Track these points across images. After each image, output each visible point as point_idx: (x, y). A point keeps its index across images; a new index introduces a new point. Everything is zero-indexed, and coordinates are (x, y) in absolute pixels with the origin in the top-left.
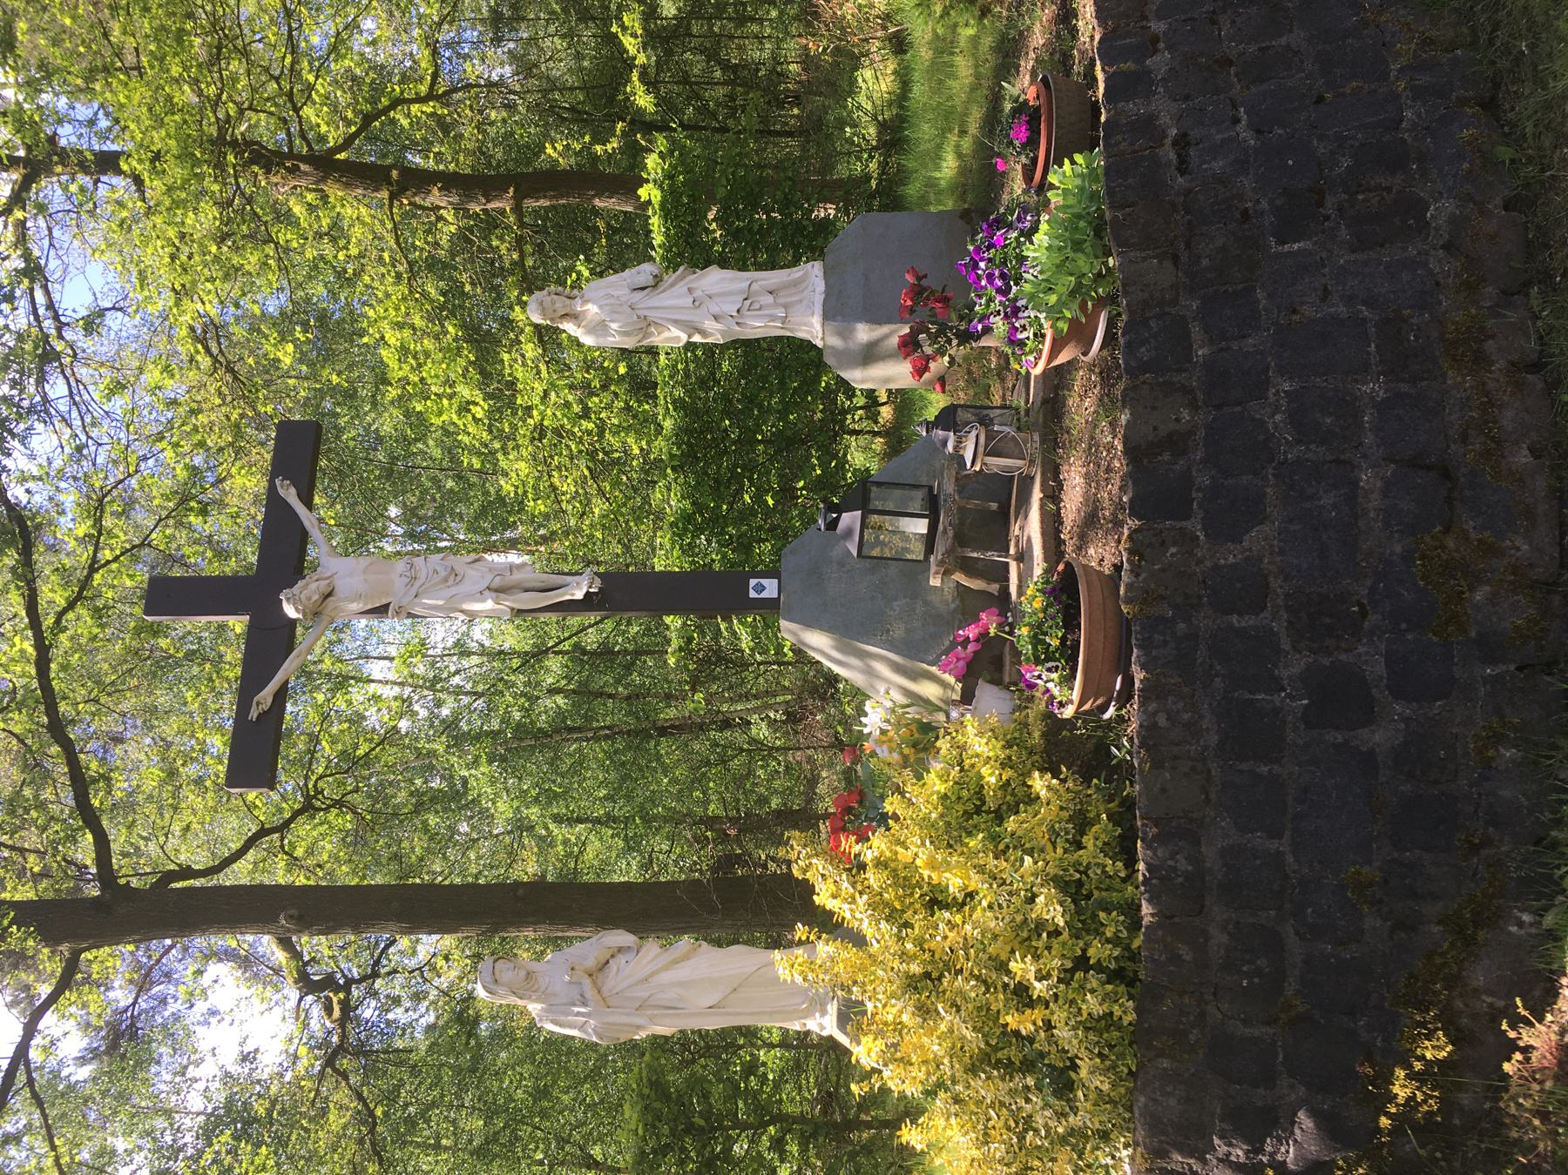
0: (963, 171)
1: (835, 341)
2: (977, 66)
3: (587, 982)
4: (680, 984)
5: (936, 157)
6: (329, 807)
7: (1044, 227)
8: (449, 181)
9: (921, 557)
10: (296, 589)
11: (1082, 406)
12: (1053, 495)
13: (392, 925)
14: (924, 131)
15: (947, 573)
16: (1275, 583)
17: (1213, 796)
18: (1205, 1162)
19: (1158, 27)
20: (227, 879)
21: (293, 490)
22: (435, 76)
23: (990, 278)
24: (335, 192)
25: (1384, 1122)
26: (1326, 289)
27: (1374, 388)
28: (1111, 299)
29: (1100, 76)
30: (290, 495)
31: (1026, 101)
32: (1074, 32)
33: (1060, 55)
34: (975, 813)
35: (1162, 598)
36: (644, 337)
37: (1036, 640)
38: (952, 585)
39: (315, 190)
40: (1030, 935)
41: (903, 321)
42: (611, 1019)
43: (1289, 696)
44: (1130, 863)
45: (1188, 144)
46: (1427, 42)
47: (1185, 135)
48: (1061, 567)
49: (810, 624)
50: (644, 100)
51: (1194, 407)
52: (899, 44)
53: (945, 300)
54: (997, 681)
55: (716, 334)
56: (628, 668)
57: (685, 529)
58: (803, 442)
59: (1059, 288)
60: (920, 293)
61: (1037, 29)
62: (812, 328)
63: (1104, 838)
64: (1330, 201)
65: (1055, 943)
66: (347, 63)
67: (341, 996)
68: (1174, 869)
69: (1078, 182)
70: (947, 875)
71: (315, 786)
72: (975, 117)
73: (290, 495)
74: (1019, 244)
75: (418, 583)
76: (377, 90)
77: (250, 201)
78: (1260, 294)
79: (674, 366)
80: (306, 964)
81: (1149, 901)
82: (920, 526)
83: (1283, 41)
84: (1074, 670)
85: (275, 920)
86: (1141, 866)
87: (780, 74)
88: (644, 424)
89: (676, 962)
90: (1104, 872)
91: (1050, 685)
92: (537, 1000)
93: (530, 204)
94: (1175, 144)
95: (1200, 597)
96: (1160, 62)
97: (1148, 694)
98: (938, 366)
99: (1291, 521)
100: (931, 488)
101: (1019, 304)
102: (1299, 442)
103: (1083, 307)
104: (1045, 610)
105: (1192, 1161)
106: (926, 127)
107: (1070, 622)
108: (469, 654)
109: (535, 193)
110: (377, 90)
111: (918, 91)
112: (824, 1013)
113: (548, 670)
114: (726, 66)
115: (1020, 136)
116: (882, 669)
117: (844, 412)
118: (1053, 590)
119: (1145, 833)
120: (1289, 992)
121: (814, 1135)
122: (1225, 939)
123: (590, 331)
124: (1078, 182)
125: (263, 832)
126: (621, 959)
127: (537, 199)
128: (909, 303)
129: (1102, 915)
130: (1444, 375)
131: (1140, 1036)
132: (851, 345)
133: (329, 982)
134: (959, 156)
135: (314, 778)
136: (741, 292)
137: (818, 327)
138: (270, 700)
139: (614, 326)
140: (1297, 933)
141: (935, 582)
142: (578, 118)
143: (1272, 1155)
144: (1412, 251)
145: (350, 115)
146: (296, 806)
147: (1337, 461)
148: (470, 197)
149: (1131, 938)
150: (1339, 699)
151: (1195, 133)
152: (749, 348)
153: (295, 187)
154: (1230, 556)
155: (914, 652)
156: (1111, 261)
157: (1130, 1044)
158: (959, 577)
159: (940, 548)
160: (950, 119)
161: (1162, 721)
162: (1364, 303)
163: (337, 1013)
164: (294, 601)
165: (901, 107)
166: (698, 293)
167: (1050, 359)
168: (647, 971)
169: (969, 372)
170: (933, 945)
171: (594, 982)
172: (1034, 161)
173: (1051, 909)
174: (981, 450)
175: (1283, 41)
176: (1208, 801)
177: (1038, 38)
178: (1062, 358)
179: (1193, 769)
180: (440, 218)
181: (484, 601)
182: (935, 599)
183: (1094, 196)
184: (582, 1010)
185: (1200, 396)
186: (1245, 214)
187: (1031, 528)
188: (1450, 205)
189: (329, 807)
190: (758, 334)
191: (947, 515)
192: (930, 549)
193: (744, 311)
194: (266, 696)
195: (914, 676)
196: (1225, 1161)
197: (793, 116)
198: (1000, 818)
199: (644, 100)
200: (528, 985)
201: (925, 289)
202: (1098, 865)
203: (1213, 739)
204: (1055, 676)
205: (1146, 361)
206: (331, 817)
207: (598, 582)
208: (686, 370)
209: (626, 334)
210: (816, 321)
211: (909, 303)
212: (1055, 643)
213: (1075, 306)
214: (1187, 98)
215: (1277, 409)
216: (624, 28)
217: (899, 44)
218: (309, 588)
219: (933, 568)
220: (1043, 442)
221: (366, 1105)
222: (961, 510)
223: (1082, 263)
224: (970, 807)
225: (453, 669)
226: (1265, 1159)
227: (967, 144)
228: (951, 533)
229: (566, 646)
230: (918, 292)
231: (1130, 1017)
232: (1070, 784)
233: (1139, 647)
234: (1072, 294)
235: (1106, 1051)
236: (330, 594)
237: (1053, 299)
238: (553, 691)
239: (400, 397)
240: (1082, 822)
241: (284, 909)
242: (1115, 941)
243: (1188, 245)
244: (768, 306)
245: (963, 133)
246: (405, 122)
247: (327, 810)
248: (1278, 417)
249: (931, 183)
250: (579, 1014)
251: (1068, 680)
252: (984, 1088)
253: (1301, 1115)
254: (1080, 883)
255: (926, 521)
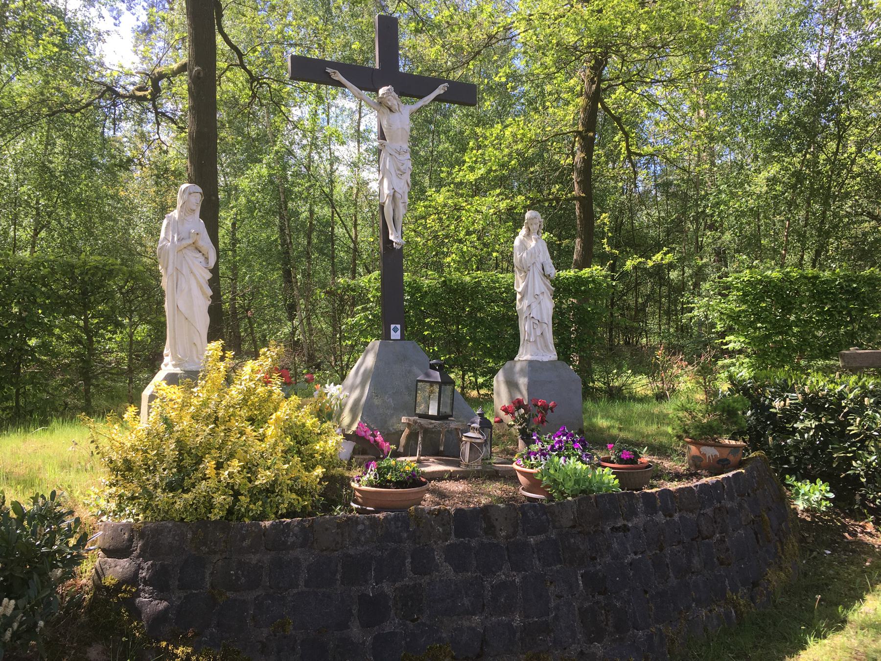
0: (601, 430)
1: (518, 367)
2: (652, 435)
3: (191, 241)
4: (190, 290)
5: (607, 416)
6: (253, 91)
7: (585, 467)
8: (588, 163)
9: (418, 411)
10: (394, 94)
11: (496, 489)
12: (452, 477)
13: (194, 128)
14: (619, 410)
15: (409, 425)
16: (427, 578)
17: (325, 553)
18: (138, 557)
19: (676, 517)
20: (219, 39)
21: (442, 92)
22: (640, 155)
23: (560, 441)
24: (581, 101)
25: (164, 644)
26: (562, 597)
27: (517, 620)
28: (551, 498)
29: (654, 490)
30: (440, 90)
31: (640, 458)
32: (671, 480)
33: (660, 474)
34: (299, 442)
35: (418, 526)
36: (519, 270)
37: (389, 468)
38: (402, 428)
39: (582, 91)
40: (250, 468)
41: (530, 400)
42: (171, 256)
43: (374, 587)
44: (287, 515)
45: (625, 532)
46: (673, 641)
47: (629, 530)
48: (423, 480)
49: (379, 357)
50: (629, 264)
51: (507, 537)
52: (660, 397)
53: (543, 421)
54: (355, 452)
55: (521, 306)
56: (321, 251)
57: (412, 288)
58: (458, 350)
59: (557, 474)
60: (544, 409)
61: (672, 463)
62: (524, 355)
63: (296, 503)
64: (601, 598)
65: (246, 481)
66: (646, 110)
67: (149, 97)
68: (288, 536)
69: (606, 481)
70: (273, 427)
71: (265, 83)
72: (629, 436)
73: (440, 90)
74: (574, 455)
75: (397, 155)
76: (634, 125)
77: (578, 59)
78: (559, 566)
79: (498, 282)
80: (169, 78)
81: (272, 524)
82: (433, 411)
83: (671, 575)
84: (376, 486)
85: (197, 64)
86: (289, 520)
87: (640, 334)
88: (464, 263)
89: (201, 288)
90: (280, 504)
91: (368, 476)
92: (180, 216)
93: (577, 205)
94: (625, 525)
95: (419, 544)
96: (660, 518)
97: (375, 522)
98: (509, 419)
99: (456, 585)
100: (451, 416)
101: (548, 456)
102: (492, 587)
103: (548, 486)
104: (405, 472)
105: (138, 551)
106: (621, 411)
107: (399, 484)
108: (331, 165)
109: (582, 207)
110: (634, 125)
111: (638, 407)
112: (175, 366)
113: (322, 208)
114: (644, 305)
115: (626, 455)
116: (355, 394)
117: (474, 371)
118: (414, 475)
119: (305, 521)
120: (228, 594)
121: (82, 360)
122: (254, 562)
123: (522, 242)
124: (606, 481)
125: (240, 55)
126: (202, 259)
127: (579, 209)
128: (539, 404)
129: (260, 503)
130: (524, 653)
131: (203, 523)
132: (517, 376)
133: (157, 90)
134: (609, 428)
135: (269, 82)
136: (542, 318)
137: (525, 358)
138: (336, 79)
139: (525, 255)
140: (258, 596)
141: (404, 419)
142: (617, 227)
143: (144, 590)
144: (579, 636)
145: (620, 110)
146: (253, 72)
147: (484, 605)
148: (580, 173)
149: (248, 517)
150: (373, 610)
151: (629, 534)
152: (513, 321)
153: (583, 81)
154: (438, 557)
155: (367, 409)
156: (570, 498)
157: (197, 519)
158: (407, 431)
159: (423, 421)
160: (626, 423)
161: (360, 527)
162: (556, 615)
163: (139, 94)
164: (388, 93)
165: (630, 398)
166: (541, 297)
167: (520, 472)
168: (196, 272)
169: (503, 435)
170: (233, 421)
171: (190, 245)
172: (613, 462)
173: (263, 478)
174: (473, 440)
175: (671, 575)
176: (322, 551)
177: (667, 464)
178: (521, 478)
179: (338, 543)
180: (568, 157)
181: (389, 189)
182: (394, 420)
183: (600, 489)
184: (176, 239)
185: (512, 540)
186: (594, 559)
187: (434, 467)
188: (600, 653)
189: (253, 91)
190: (521, 328)
191: (439, 424)
192: (421, 416)
193: (533, 320)
194: (338, 77)
195: (354, 411)
196: (139, 567)
197: (619, 341)
198: (299, 453)
199: (629, 264)
200: (186, 210)
201: (546, 412)
202: (283, 500)
203: (351, 552)
204: (372, 478)
205: (524, 515)
206: (247, 91)
207: (398, 247)
208: (495, 288)
209: (521, 260)
210: (528, 357)
211: (539, 404)
212: (389, 477)
213: (548, 482)
214: (645, 530)
215: (507, 576)
216: (665, 254)
217: (660, 397)
218: (394, 100)
219: (412, 418)
220: (478, 471)
221: (83, 108)
222: (439, 432)
223: (569, 484)
224: (300, 438)
225: (322, 154)
226: (141, 587)
227: (615, 432)
228: (431, 426)
229: (336, 218)
230: (545, 408)
231: (213, 517)
232: (319, 487)
233: (395, 515)
234: (555, 480)
235: (194, 506)
236: (391, 110)
237: (552, 471)
238: (312, 212)
239: (476, 134)
240: (301, 492)
241: (204, 69)
242: (248, 510)
243: (580, 532)
244: (535, 333)
245: (620, 429)
246: (616, 139)
247: (251, 89)
248: (503, 577)
249: (595, 415)
250: (173, 237)
251: (370, 484)
252: (170, 449)
253: (165, 603)
254: (273, 492)
255: (436, 414)
